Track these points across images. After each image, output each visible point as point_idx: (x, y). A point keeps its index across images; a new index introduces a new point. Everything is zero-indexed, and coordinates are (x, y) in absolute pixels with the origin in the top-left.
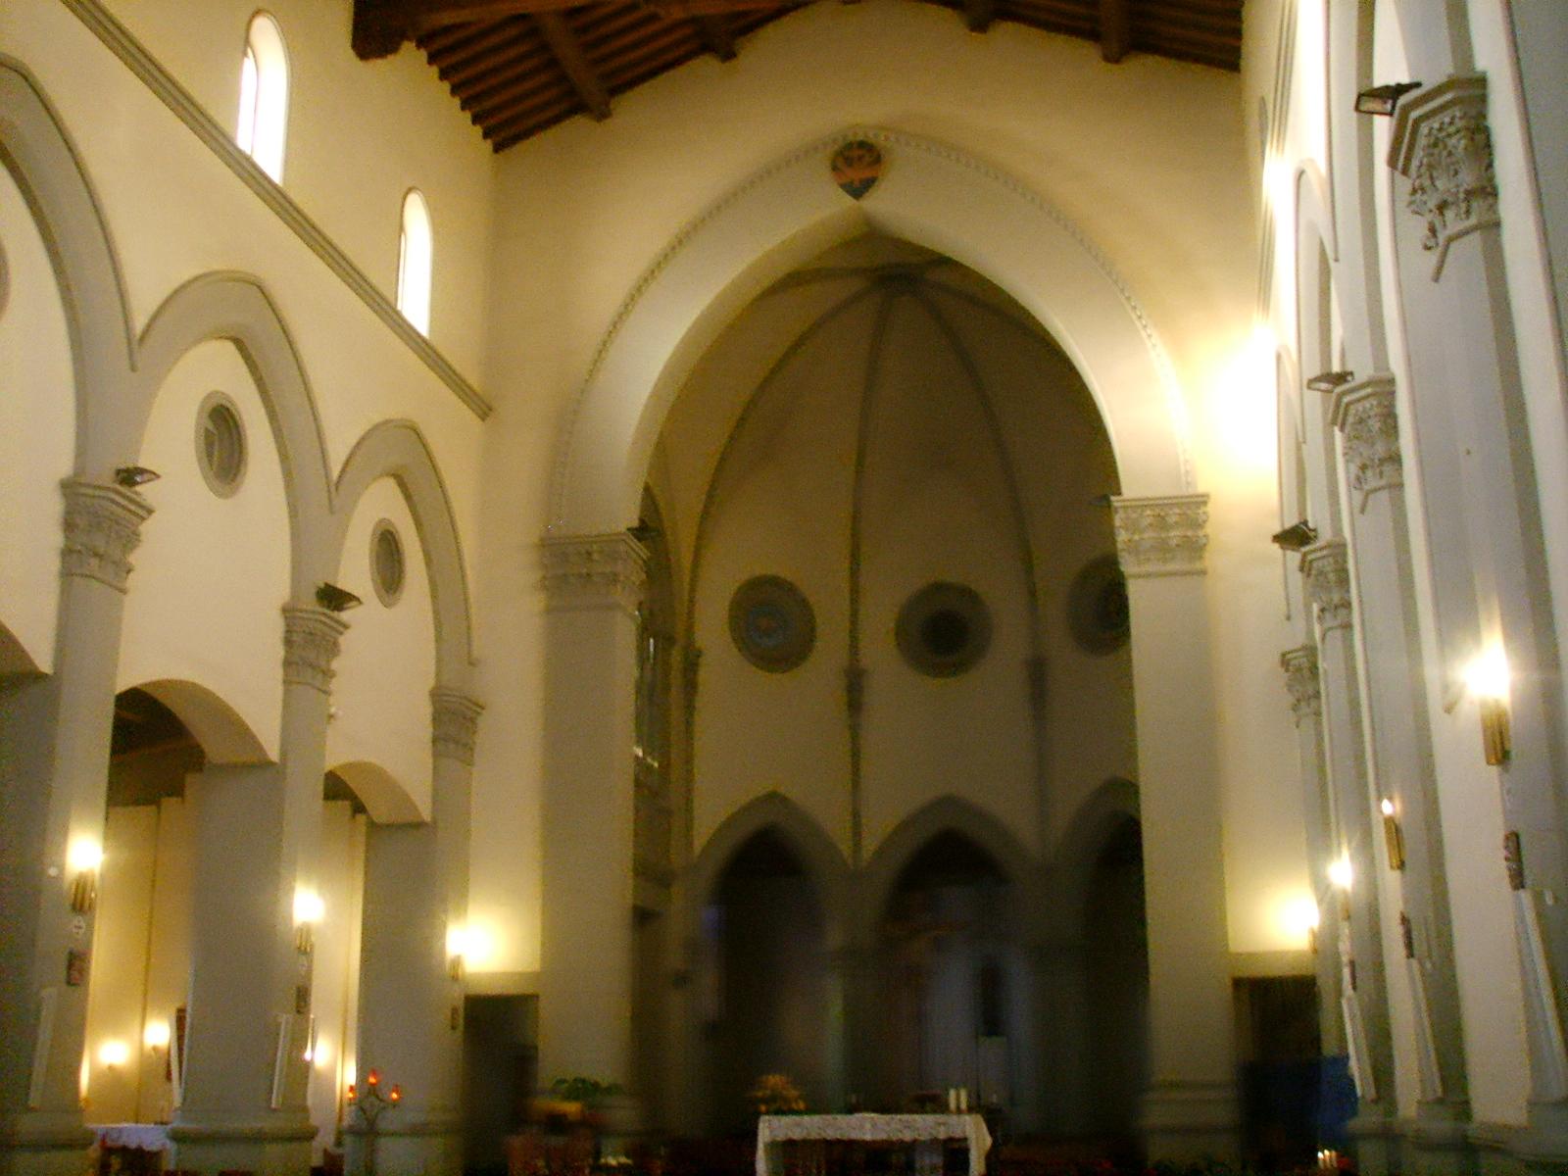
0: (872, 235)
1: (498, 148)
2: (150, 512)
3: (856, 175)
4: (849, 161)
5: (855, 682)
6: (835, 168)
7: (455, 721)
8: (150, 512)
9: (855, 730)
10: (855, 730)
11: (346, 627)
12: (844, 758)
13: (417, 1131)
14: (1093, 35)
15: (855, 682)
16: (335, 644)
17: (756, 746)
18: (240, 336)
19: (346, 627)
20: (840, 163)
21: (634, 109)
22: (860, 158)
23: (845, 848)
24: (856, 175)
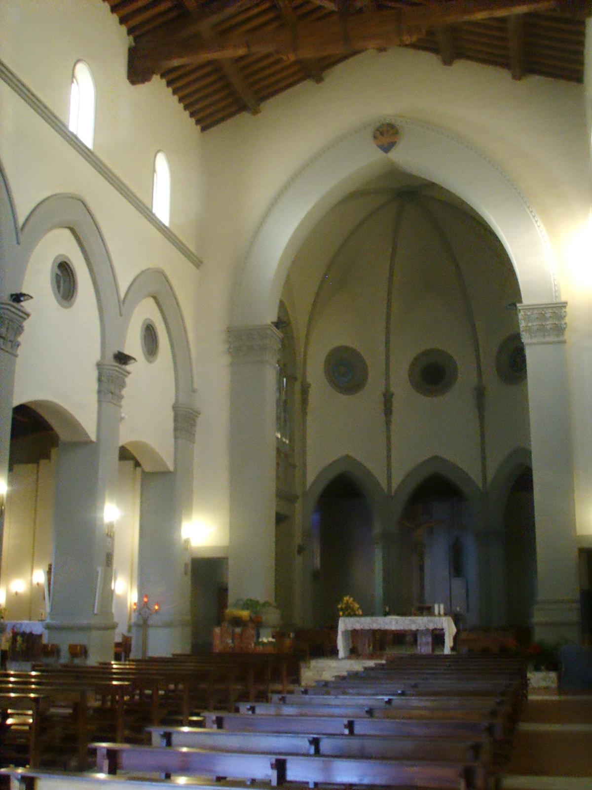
0: (394, 173)
1: (204, 129)
2: (28, 315)
3: (385, 140)
4: (382, 133)
5: (388, 399)
6: (375, 137)
7: (185, 421)
8: (28, 315)
9: (388, 422)
10: (388, 422)
11: (129, 373)
12: (391, 440)
13: (168, 625)
14: (506, 65)
15: (388, 399)
16: (124, 382)
17: (337, 433)
18: (71, 226)
19: (129, 373)
20: (378, 134)
21: (269, 107)
22: (388, 131)
23: (384, 485)
24: (385, 140)
